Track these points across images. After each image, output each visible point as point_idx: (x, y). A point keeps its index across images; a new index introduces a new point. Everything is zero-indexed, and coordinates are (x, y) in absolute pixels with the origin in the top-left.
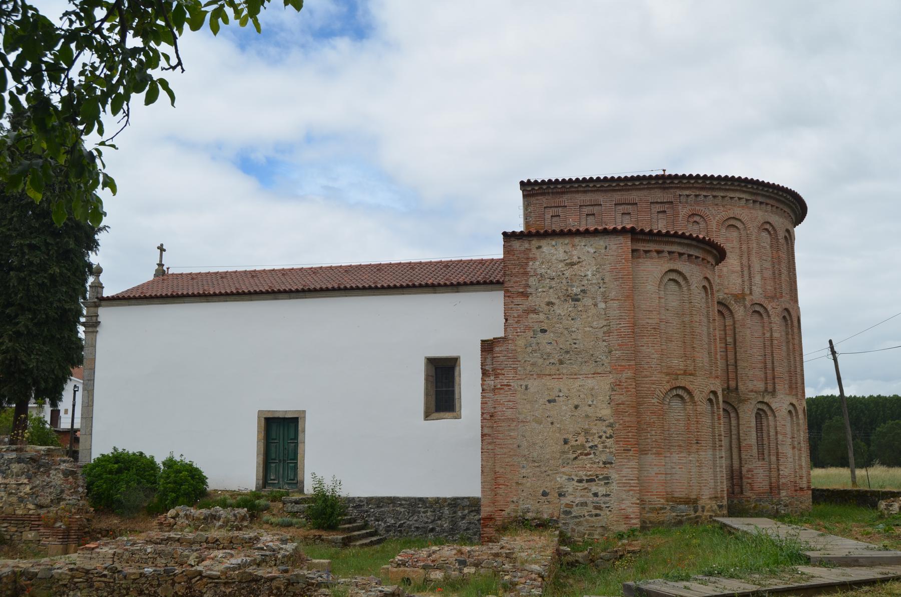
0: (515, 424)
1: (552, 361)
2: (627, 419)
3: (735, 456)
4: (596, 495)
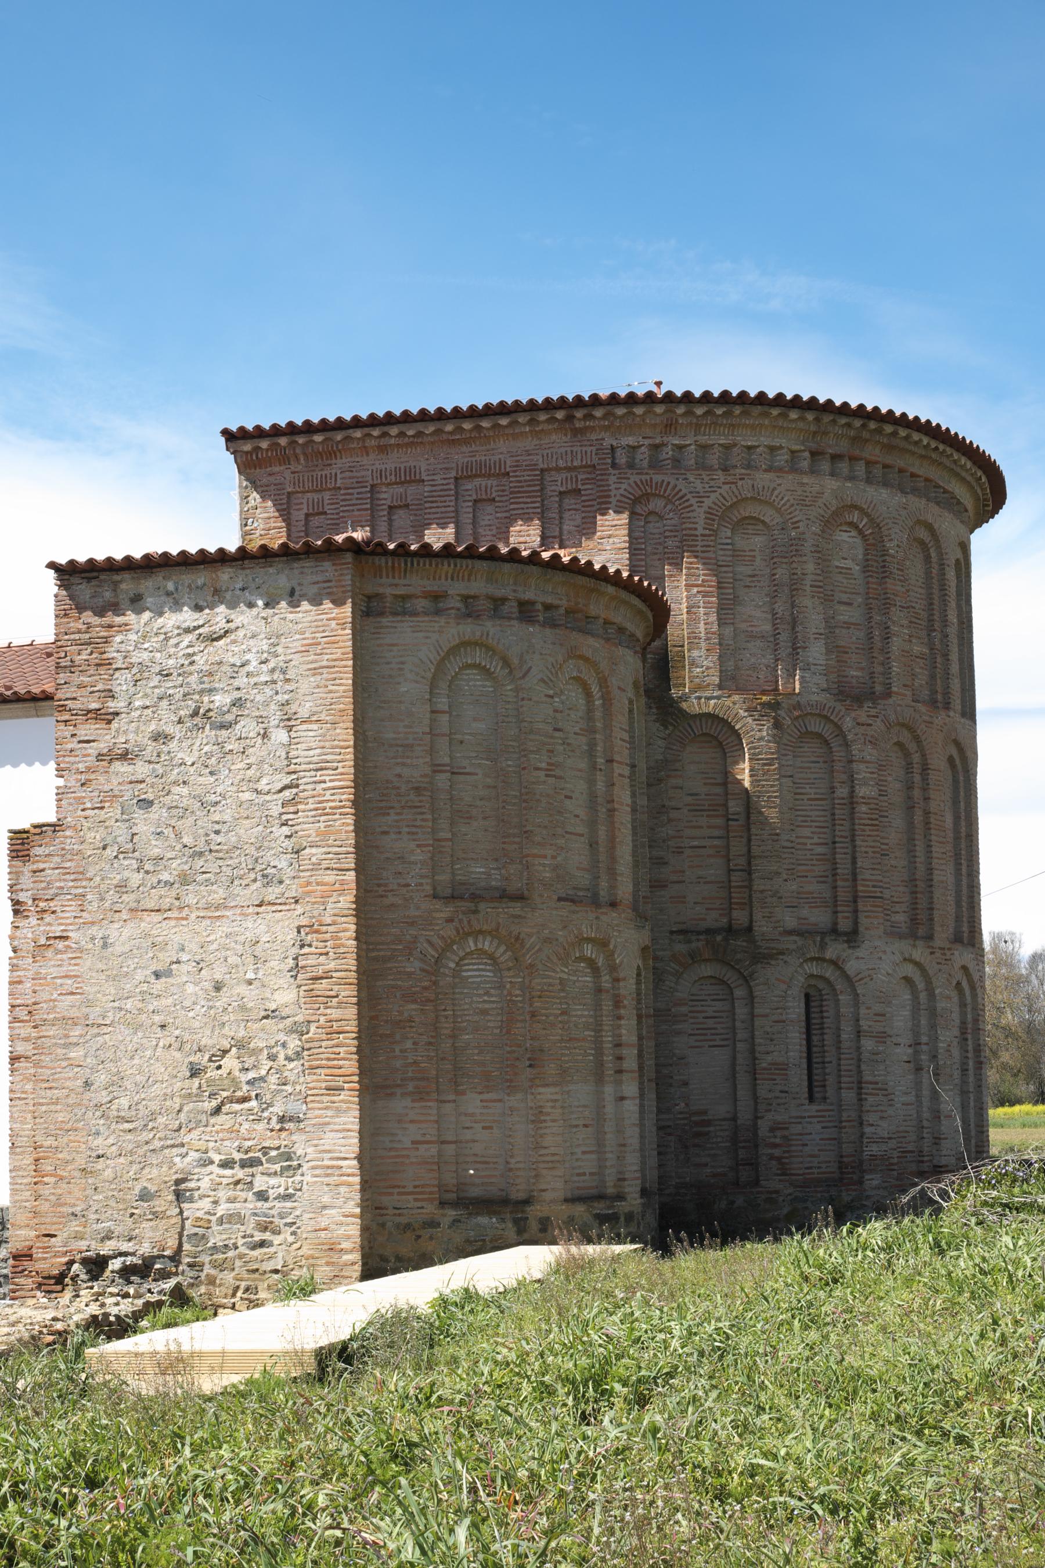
0: (77, 1031)
1: (165, 876)
2: (335, 1014)
3: (743, 1093)
4: (262, 1196)
